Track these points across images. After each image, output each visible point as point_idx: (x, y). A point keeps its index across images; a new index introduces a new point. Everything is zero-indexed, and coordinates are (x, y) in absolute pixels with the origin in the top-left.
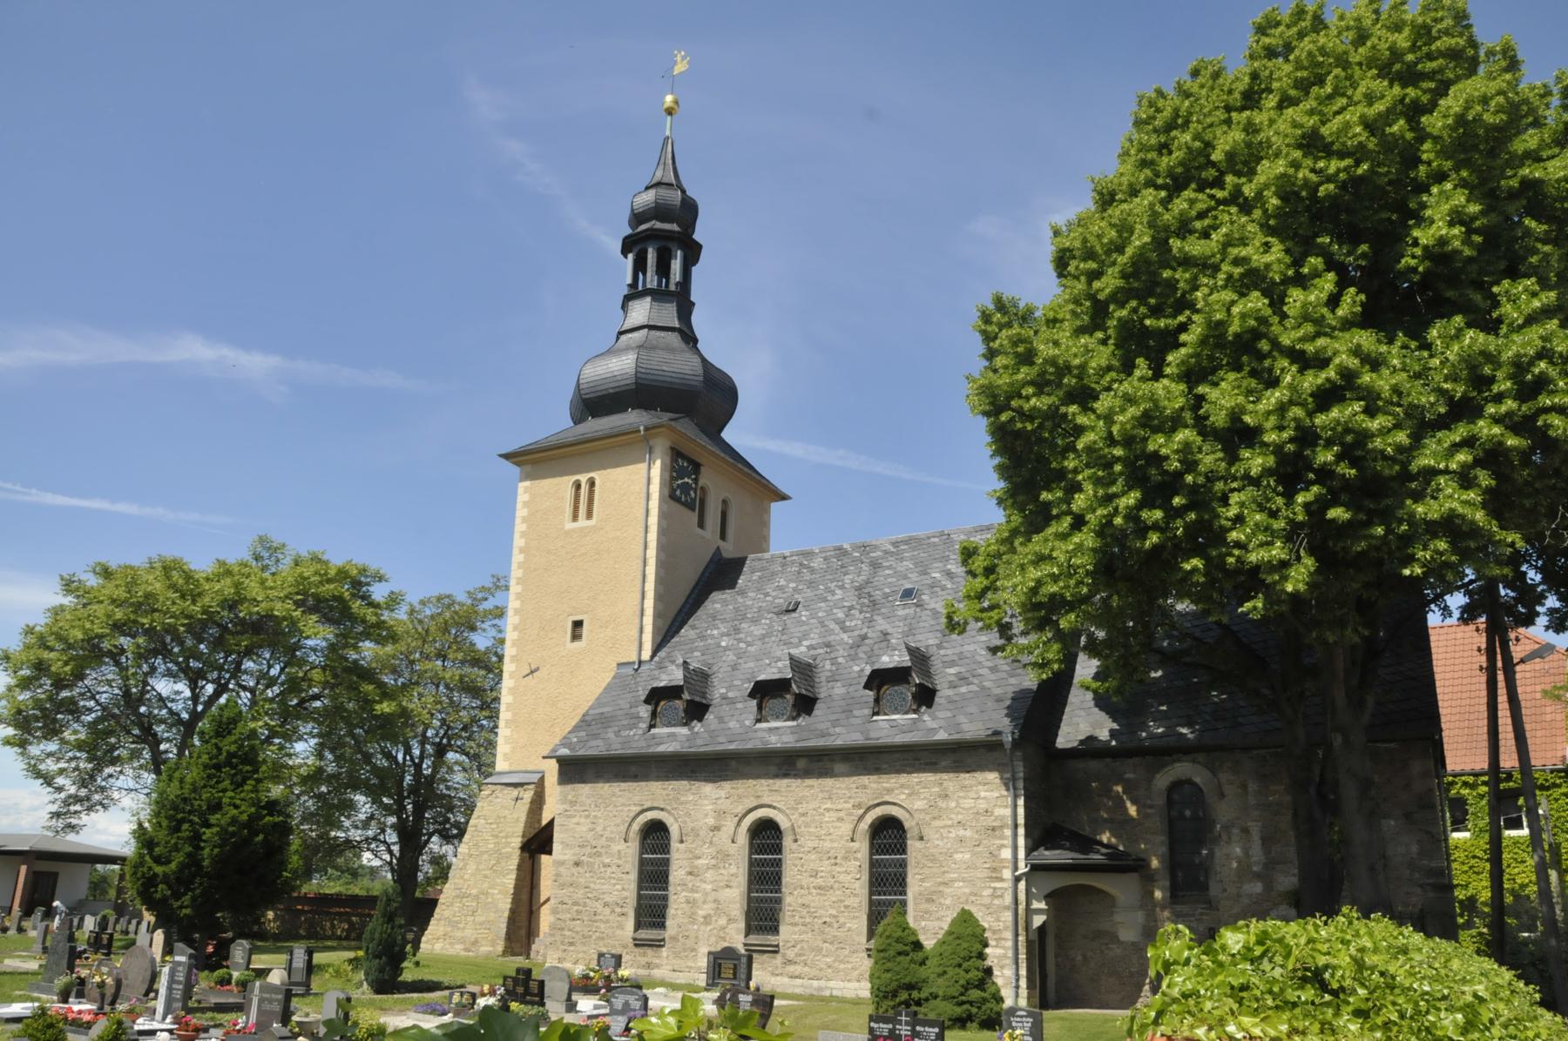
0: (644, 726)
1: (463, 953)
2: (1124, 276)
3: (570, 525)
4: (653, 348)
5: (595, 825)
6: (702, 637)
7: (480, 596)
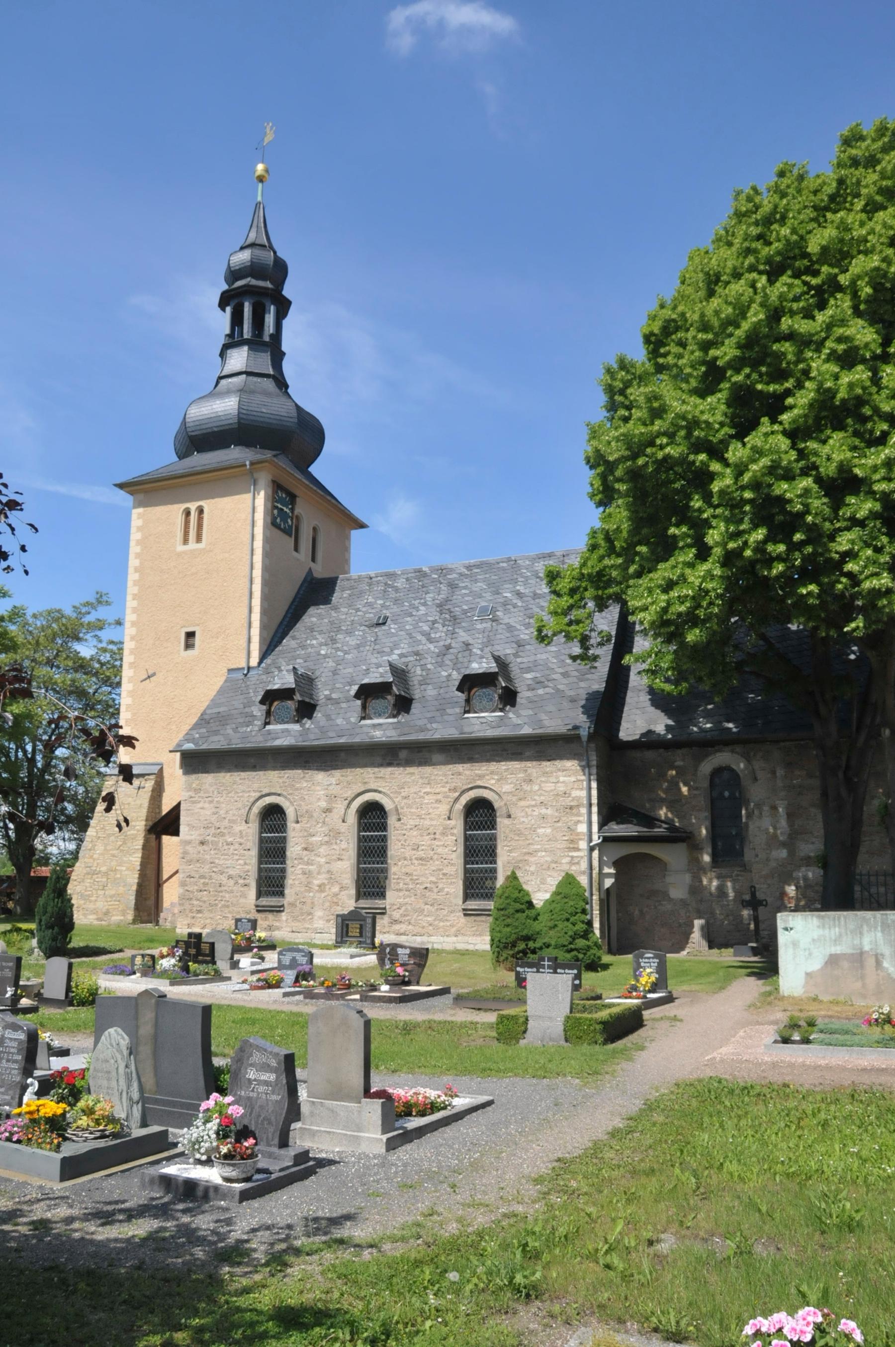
0: (258, 723)
1: (96, 922)
2: (739, 346)
3: (181, 548)
4: (252, 392)
5: (218, 810)
6: (303, 647)
7: (83, 611)
